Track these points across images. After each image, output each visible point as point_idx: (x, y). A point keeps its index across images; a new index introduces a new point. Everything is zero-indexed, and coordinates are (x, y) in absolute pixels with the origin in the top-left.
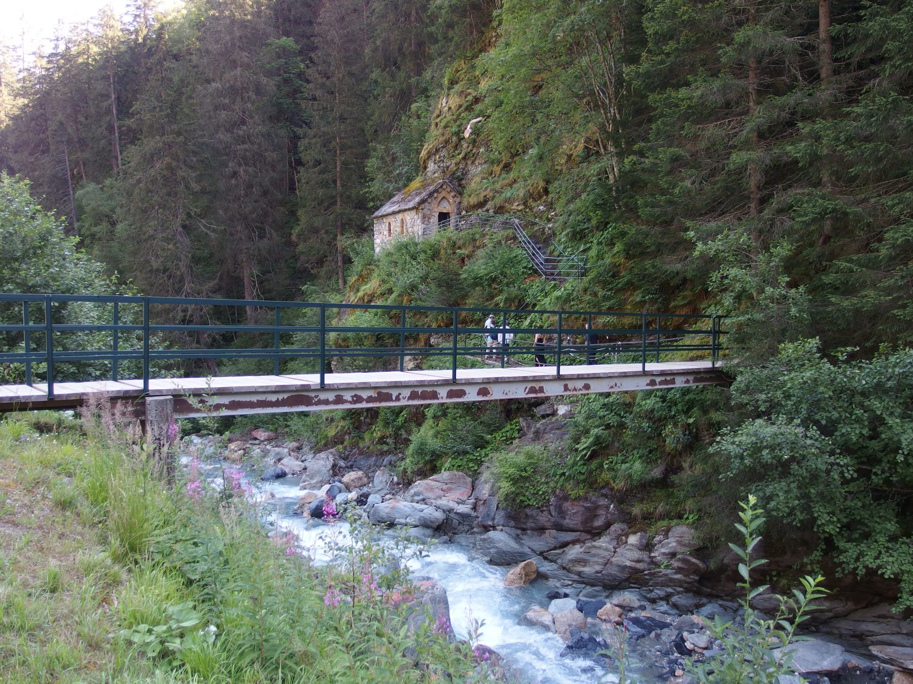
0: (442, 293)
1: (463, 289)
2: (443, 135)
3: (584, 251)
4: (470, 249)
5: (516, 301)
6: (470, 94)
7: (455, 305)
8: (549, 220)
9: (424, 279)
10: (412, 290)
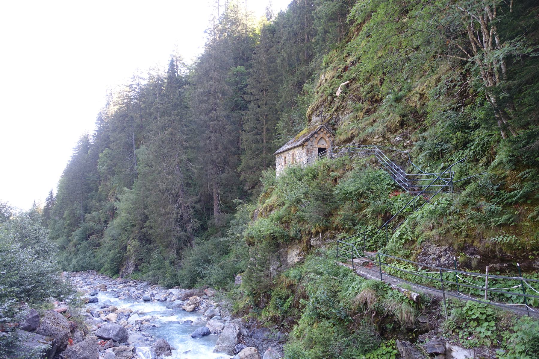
0: (319, 206)
2: (322, 97)
3: (443, 168)
4: (341, 171)
5: (383, 213)
6: (340, 68)
8: (405, 147)
9: (306, 195)
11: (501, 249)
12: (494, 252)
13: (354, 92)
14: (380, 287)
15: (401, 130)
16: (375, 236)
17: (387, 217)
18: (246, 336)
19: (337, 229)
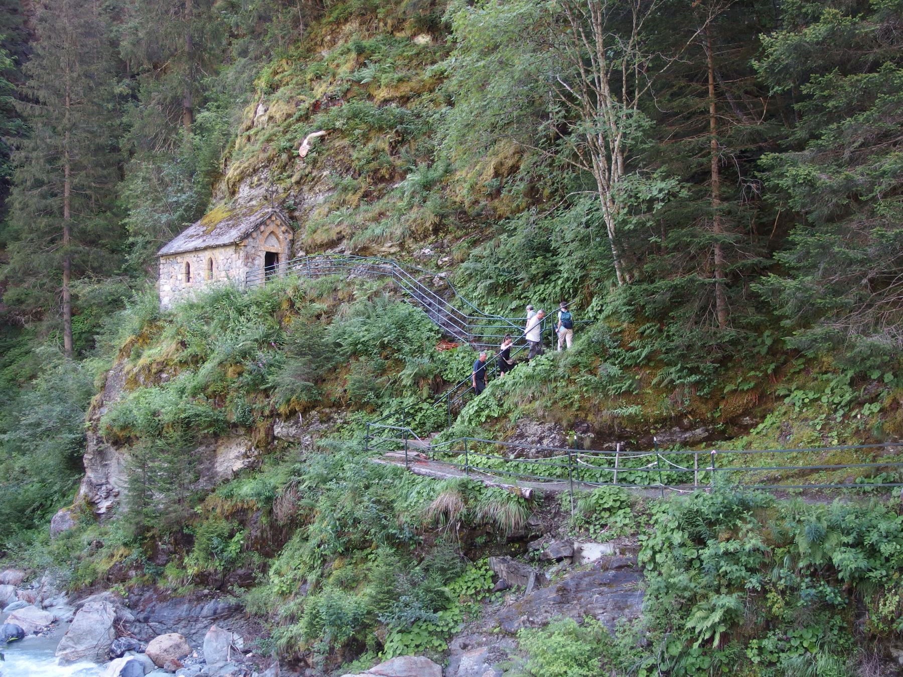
8: (439, 268)
11: (620, 423)
12: (611, 427)
13: (337, 154)
14: (470, 487)
15: (433, 237)
16: (420, 415)
17: (439, 385)
18: (132, 623)
19: (337, 405)
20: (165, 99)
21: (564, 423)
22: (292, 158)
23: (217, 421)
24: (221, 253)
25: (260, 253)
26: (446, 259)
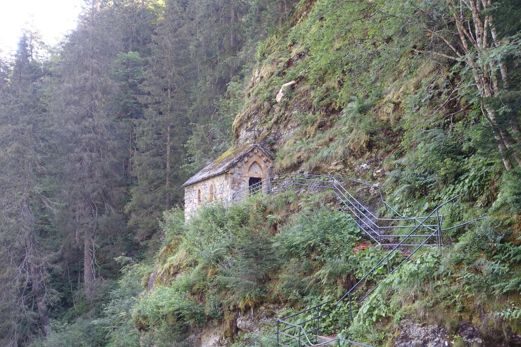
0: (250, 266)
1: (274, 260)
2: (255, 102)
4: (284, 213)
5: (344, 276)
6: (281, 61)
7: (264, 280)
8: (374, 179)
9: (230, 249)
10: (217, 262)
11: (509, 328)
13: (302, 96)
15: (368, 153)
17: (351, 283)
19: (277, 302)
20: (215, 80)
21: (448, 326)
22: (272, 105)
23: (195, 313)
24: (217, 181)
25: (244, 179)
26: (379, 171)
